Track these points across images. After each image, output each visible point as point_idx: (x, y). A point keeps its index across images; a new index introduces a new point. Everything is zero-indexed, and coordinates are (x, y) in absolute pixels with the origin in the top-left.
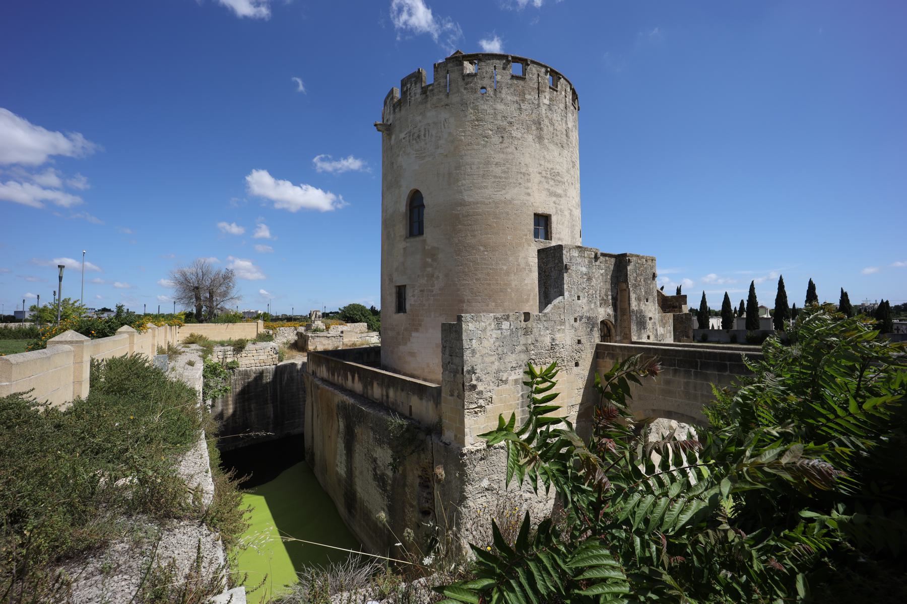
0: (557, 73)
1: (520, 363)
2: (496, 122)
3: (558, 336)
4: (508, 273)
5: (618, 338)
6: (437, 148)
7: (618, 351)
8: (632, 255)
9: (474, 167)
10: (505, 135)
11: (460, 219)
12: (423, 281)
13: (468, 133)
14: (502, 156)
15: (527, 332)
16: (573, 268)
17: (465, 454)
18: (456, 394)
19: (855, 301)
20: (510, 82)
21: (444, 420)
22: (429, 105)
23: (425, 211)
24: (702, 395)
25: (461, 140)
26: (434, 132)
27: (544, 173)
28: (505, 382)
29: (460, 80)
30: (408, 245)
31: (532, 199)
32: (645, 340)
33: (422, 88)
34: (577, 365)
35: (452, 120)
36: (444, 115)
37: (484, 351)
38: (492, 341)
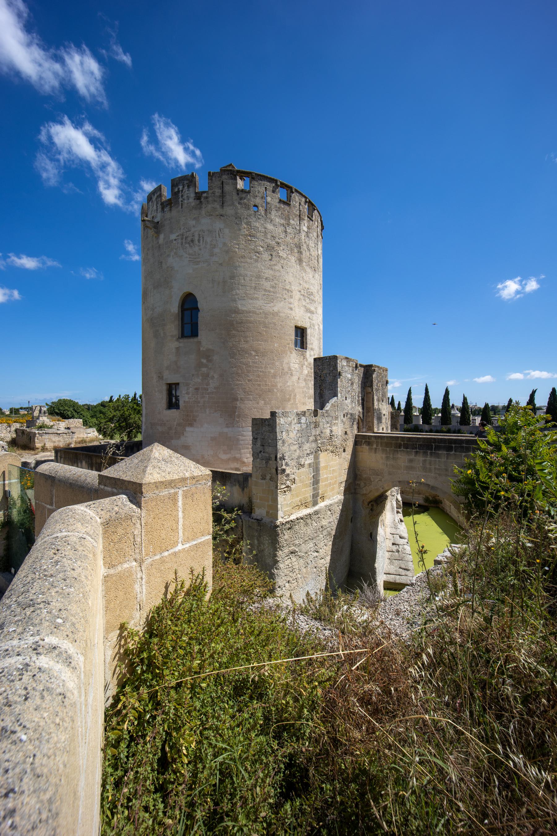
0: (312, 205)
1: (312, 450)
2: (266, 241)
3: (334, 428)
4: (274, 376)
5: (364, 430)
6: (212, 255)
7: (373, 439)
8: (376, 366)
9: (247, 279)
10: (274, 254)
11: (234, 326)
12: (198, 380)
13: (241, 246)
14: (271, 272)
15: (316, 425)
16: (343, 374)
17: (278, 526)
18: (268, 477)
19: (471, 403)
20: (278, 205)
21: (254, 500)
22: (203, 212)
23: (200, 315)
24: (435, 468)
25: (235, 252)
26: (209, 240)
27: (302, 291)
28: (303, 466)
29: (234, 193)
30: (181, 345)
31: (293, 313)
32: (381, 431)
33: (196, 193)
34: (344, 451)
35: (227, 231)
36: (219, 224)
37: (290, 441)
38: (295, 432)
